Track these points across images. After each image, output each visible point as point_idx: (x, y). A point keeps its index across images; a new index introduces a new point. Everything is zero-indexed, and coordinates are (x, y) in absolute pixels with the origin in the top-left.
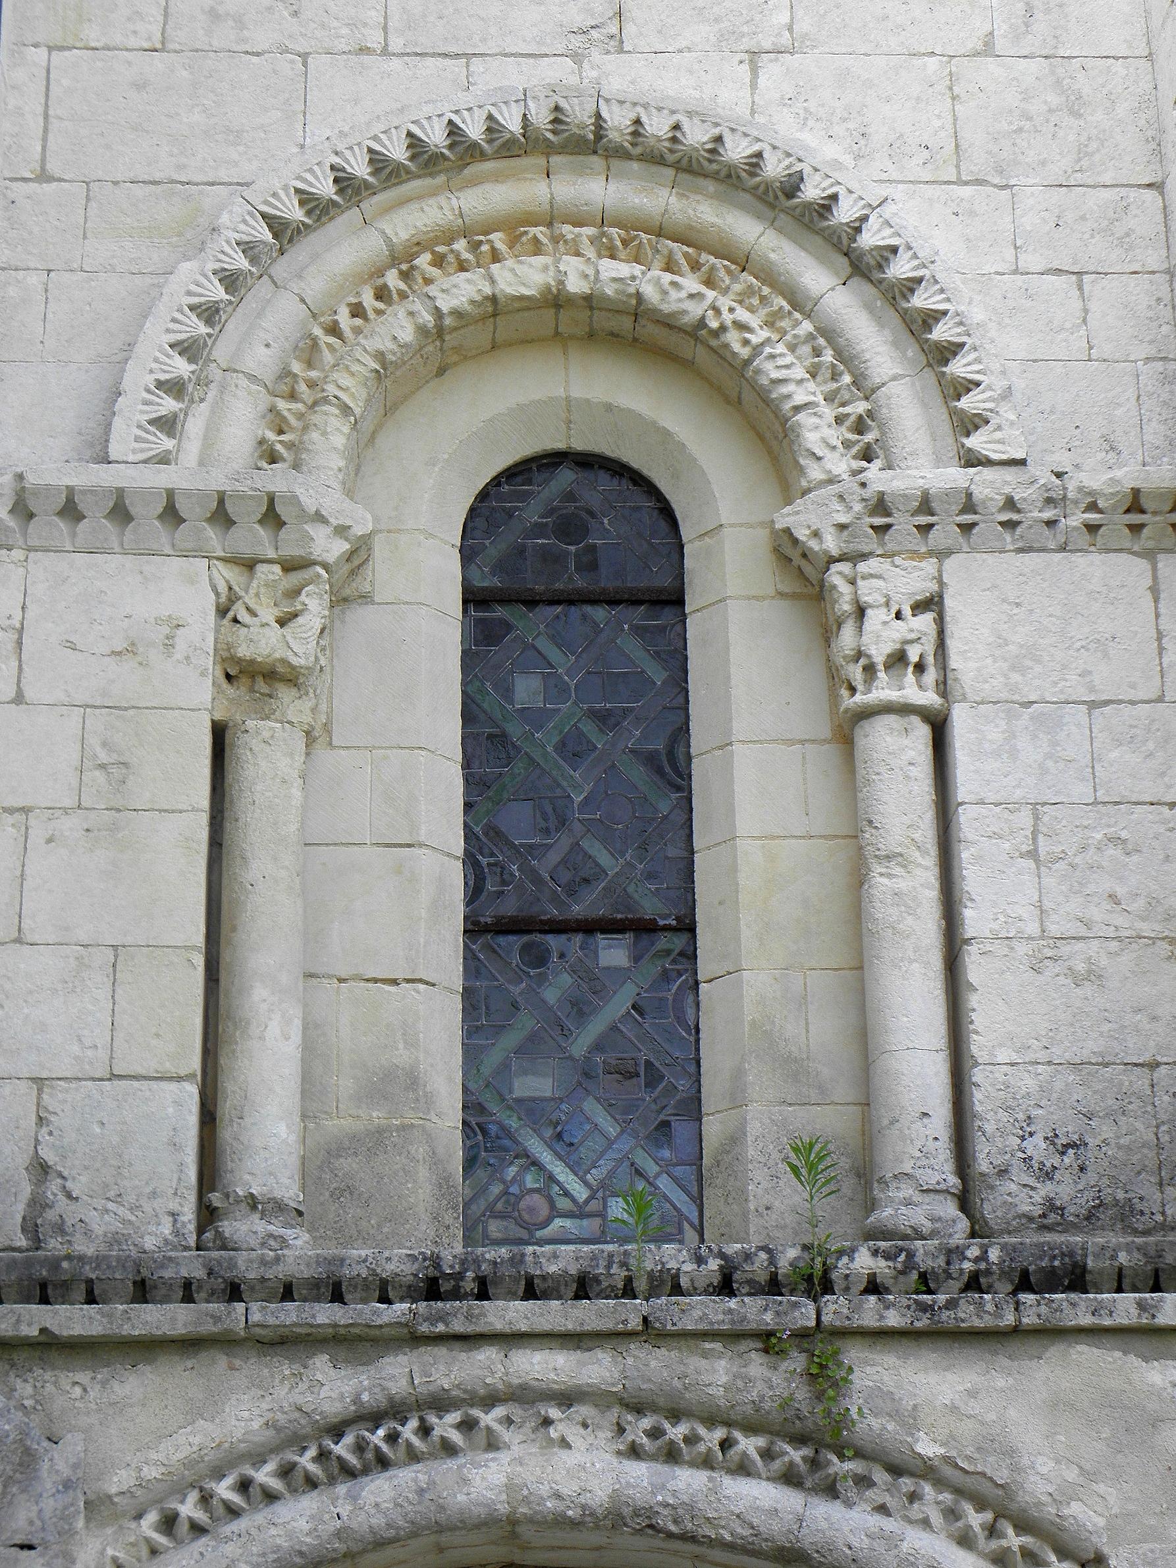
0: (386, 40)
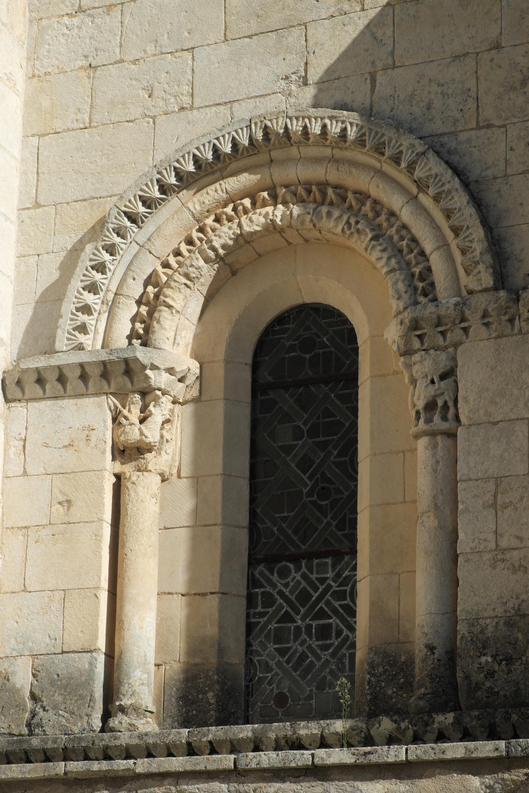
0: (192, 102)
